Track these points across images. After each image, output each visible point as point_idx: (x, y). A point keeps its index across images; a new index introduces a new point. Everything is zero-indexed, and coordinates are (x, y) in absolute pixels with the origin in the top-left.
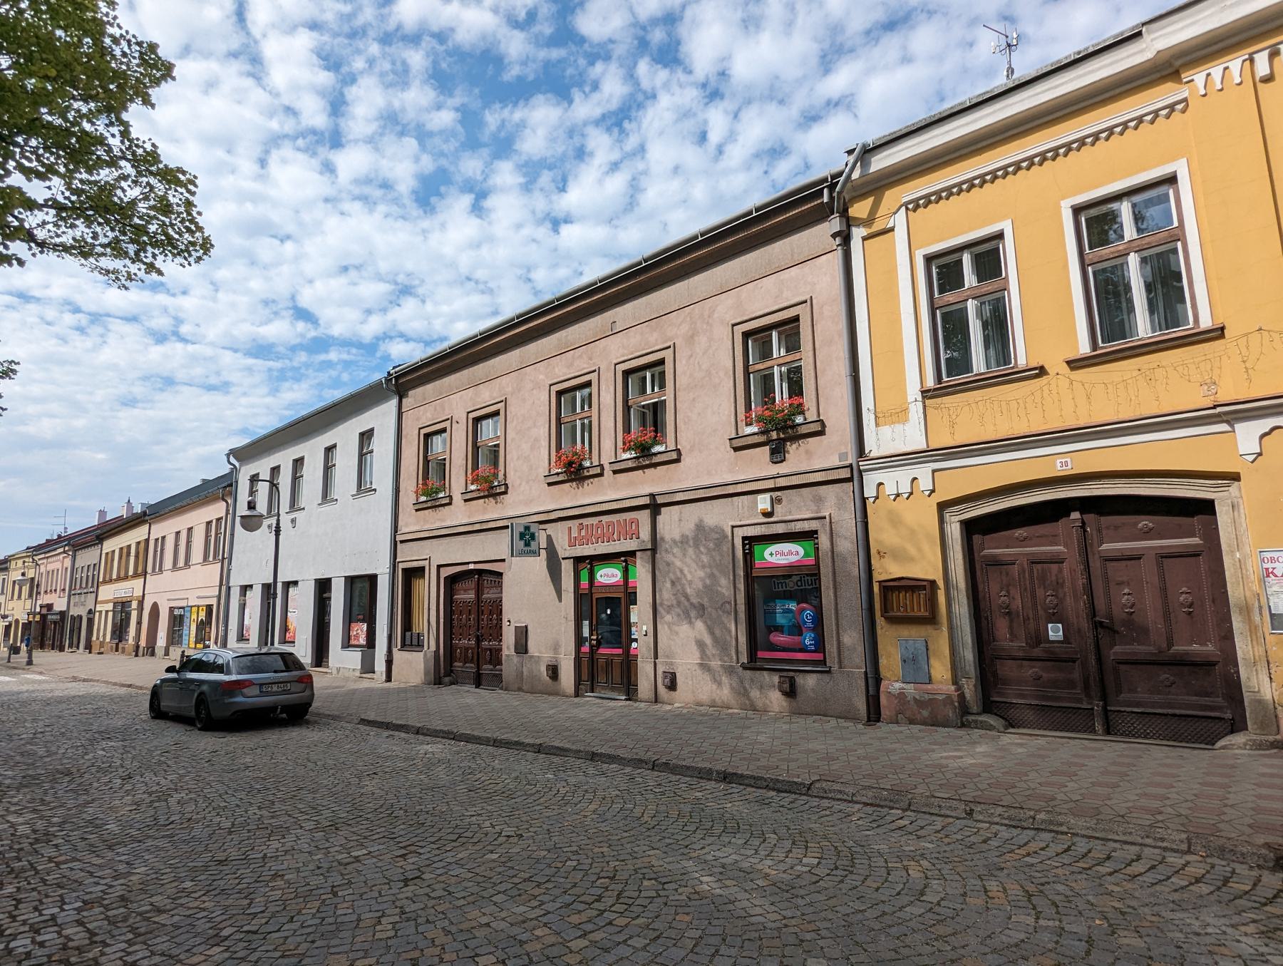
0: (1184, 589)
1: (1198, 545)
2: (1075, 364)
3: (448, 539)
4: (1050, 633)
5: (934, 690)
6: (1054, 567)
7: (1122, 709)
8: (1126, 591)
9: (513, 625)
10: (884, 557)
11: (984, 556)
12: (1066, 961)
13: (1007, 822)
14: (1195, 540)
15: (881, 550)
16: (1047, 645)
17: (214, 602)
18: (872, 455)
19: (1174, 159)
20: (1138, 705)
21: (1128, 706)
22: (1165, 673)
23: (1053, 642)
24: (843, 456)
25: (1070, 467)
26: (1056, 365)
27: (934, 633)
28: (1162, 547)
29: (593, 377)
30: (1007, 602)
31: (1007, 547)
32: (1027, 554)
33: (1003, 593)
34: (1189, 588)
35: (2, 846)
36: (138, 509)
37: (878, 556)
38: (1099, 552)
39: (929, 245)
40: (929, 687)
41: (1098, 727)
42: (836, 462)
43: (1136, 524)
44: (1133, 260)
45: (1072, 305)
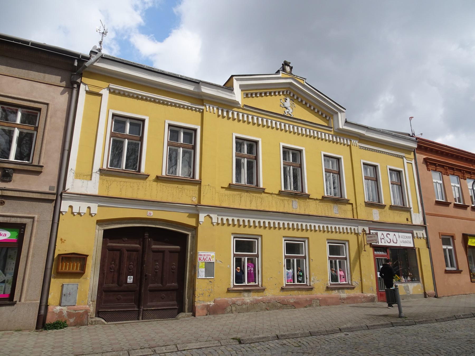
2: (159, 179)
4: (128, 280)
6: (135, 253)
7: (148, 309)
10: (64, 242)
11: (109, 246)
12: (340, 355)
13: (169, 351)
15: (63, 238)
16: (126, 285)
17: (97, 205)
18: (68, 191)
19: (146, 115)
24: (51, 188)
26: (153, 177)
28: (170, 248)
29: (43, 107)
32: (126, 247)
33: (113, 263)
35: (474, 327)
37: (60, 241)
39: (116, 110)
40: (75, 307)
42: (47, 190)
44: (126, 141)
45: (263, 171)
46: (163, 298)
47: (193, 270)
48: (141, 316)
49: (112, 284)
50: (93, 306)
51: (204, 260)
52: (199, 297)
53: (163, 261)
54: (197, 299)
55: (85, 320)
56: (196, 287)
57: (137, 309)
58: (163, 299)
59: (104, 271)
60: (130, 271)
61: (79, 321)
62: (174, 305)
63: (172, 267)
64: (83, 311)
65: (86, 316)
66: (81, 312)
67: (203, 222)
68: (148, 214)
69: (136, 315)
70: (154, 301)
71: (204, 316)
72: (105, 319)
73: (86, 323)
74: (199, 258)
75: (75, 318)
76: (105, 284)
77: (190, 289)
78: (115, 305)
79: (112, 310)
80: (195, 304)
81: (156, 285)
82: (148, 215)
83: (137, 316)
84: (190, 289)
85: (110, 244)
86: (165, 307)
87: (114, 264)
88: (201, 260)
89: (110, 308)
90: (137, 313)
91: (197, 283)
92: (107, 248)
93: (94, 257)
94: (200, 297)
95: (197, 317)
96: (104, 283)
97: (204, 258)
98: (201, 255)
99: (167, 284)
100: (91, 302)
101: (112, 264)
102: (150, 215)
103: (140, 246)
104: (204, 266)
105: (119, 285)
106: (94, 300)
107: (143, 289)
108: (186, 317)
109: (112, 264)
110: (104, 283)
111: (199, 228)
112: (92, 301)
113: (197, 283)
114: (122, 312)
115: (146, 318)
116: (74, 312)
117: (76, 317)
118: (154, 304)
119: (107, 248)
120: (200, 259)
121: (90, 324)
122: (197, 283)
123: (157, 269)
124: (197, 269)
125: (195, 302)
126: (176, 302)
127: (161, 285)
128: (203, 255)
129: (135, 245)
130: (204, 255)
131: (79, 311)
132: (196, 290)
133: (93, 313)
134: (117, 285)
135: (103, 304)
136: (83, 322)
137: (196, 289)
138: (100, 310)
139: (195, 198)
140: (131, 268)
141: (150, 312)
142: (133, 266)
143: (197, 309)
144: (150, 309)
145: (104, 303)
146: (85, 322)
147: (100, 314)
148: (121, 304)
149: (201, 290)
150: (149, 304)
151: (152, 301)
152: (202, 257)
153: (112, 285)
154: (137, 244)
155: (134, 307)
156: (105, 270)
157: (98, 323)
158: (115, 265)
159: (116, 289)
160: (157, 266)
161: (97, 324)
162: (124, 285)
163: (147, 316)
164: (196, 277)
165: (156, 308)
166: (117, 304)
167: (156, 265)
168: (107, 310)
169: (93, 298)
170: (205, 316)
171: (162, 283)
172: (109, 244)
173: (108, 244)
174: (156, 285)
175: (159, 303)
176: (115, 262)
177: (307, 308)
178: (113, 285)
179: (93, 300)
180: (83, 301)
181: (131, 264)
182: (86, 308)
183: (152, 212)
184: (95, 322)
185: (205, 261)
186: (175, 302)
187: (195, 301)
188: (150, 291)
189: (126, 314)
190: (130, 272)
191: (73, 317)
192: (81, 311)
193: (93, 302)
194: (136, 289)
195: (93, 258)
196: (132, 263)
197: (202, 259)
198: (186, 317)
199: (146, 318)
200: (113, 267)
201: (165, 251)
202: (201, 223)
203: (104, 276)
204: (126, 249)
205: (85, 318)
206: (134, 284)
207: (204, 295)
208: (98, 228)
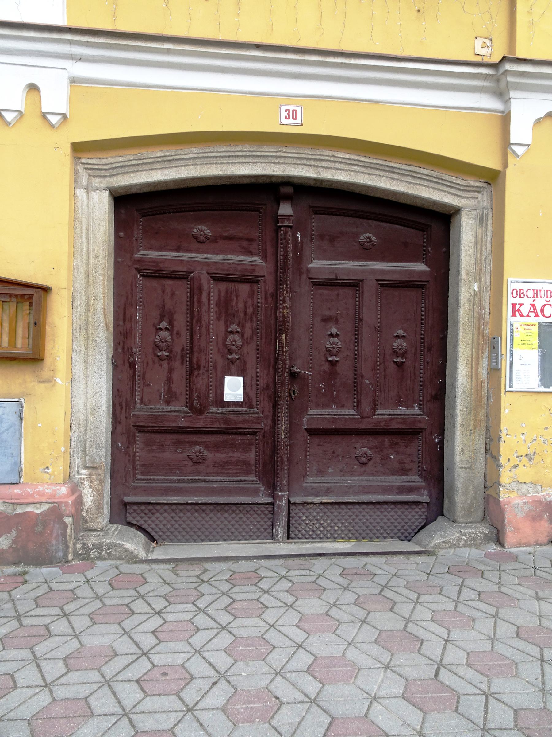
0: (401, 332)
1: (423, 272)
3: (546, 394)
5: (28, 495)
6: (244, 288)
7: (310, 500)
8: (334, 331)
9: (35, 295)
11: (140, 261)
14: (420, 267)
16: (220, 410)
20: (328, 492)
21: (317, 495)
22: (363, 447)
23: (229, 404)
25: (299, 121)
27: (41, 388)
28: (383, 272)
30: (169, 339)
31: (178, 249)
32: (207, 264)
33: (164, 324)
34: (405, 331)
36: (13, 305)
38: (308, 271)
40: (17, 490)
41: (281, 531)
43: (357, 235)
46: (364, 460)
47: (486, 355)
48: (284, 527)
49: (168, 403)
50: (90, 486)
51: (536, 316)
52: (514, 467)
53: (359, 320)
54: (506, 477)
55: (55, 545)
56: (503, 427)
57: (269, 500)
58: (364, 464)
59: (132, 354)
60: (230, 357)
61: (31, 546)
62: (410, 490)
63: (395, 344)
64: (45, 508)
65: (57, 530)
66: (38, 512)
67: (528, 145)
68: (284, 114)
69: (265, 522)
70: (330, 470)
71: (541, 545)
72: (149, 530)
73: (60, 554)
74: (514, 305)
75: (14, 533)
76: (142, 402)
77: (471, 434)
78: (183, 480)
79: (174, 499)
80: (501, 494)
81: (333, 411)
82: (284, 120)
83: (269, 523)
84: (471, 434)
85: (145, 253)
86: (373, 493)
87: (167, 329)
88: (522, 315)
89: (167, 491)
90: (266, 512)
91: (505, 411)
92: (137, 266)
93: (78, 297)
94: (521, 465)
95: (513, 550)
96: (138, 401)
97: (533, 306)
98: (521, 293)
99: (379, 411)
100: (84, 471)
101: (161, 329)
102: (291, 121)
103: (266, 261)
104: (535, 341)
105: (191, 407)
106: (96, 465)
107: (283, 427)
108: (461, 543)
109: (161, 329)
110: (138, 401)
111: (510, 172)
112: (86, 467)
113: (507, 411)
114: (212, 507)
115: (303, 532)
116: (9, 510)
117: (17, 530)
118: (327, 481)
119: (136, 269)
120: (516, 311)
121: (76, 555)
122: (507, 411)
123: (335, 350)
124: (503, 353)
125: (501, 489)
126: (416, 478)
127: (352, 412)
128: (530, 294)
129: (241, 258)
130: (536, 294)
131: (29, 509)
132: (499, 438)
133: (94, 511)
134: (186, 409)
135: (139, 477)
136: (47, 551)
137: (503, 435)
138: (127, 499)
139: (485, 40)
140: (234, 347)
141: (318, 513)
142: (242, 336)
143: (508, 516)
144: (317, 500)
145: (143, 473)
146: (57, 551)
147: (132, 511)
148: (205, 480)
149: (523, 438)
150: (311, 481)
151: (321, 472)
152: (527, 302)
153: (165, 407)
154: (251, 254)
155: (256, 492)
156: (134, 350)
157: (109, 554)
158: (171, 334)
159: (182, 423)
160: (336, 340)
161: (105, 559)
162: (213, 409)
163: (307, 524)
164: (503, 386)
165: (340, 499)
166: (192, 480)
167: (331, 336)
168: (152, 499)
169: (91, 457)
170: (544, 548)
171: (357, 405)
172: (142, 252)
173: (139, 251)
174: (333, 411)
175: (350, 480)
176: (171, 323)
177: (129, 369)
178: (169, 408)
179: (92, 461)
180: (47, 468)
181: (232, 332)
182: (53, 496)
183: (299, 110)
184: (98, 549)
185: (541, 319)
186: (415, 479)
187: (500, 485)
188: (313, 433)
189: (226, 515)
190: (232, 362)
191: (9, 532)
192: (38, 508)
193: (94, 472)
194: (258, 426)
195: (77, 303)
196: (234, 327)
197: (525, 310)
198: (461, 543)
199: (303, 532)
200: (163, 340)
201: (362, 280)
202: (520, 150)
203: (134, 375)
204: (208, 273)
205: (55, 534)
206: (251, 406)
207: (537, 459)
208: (85, 182)
